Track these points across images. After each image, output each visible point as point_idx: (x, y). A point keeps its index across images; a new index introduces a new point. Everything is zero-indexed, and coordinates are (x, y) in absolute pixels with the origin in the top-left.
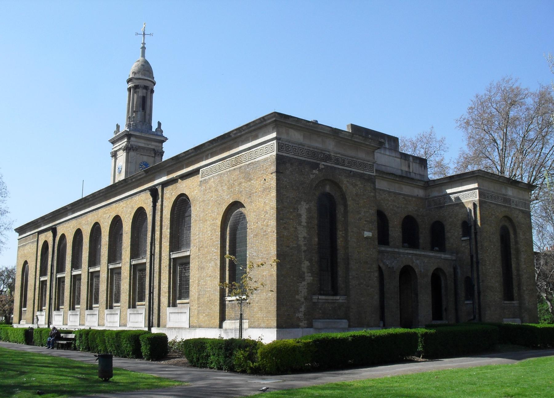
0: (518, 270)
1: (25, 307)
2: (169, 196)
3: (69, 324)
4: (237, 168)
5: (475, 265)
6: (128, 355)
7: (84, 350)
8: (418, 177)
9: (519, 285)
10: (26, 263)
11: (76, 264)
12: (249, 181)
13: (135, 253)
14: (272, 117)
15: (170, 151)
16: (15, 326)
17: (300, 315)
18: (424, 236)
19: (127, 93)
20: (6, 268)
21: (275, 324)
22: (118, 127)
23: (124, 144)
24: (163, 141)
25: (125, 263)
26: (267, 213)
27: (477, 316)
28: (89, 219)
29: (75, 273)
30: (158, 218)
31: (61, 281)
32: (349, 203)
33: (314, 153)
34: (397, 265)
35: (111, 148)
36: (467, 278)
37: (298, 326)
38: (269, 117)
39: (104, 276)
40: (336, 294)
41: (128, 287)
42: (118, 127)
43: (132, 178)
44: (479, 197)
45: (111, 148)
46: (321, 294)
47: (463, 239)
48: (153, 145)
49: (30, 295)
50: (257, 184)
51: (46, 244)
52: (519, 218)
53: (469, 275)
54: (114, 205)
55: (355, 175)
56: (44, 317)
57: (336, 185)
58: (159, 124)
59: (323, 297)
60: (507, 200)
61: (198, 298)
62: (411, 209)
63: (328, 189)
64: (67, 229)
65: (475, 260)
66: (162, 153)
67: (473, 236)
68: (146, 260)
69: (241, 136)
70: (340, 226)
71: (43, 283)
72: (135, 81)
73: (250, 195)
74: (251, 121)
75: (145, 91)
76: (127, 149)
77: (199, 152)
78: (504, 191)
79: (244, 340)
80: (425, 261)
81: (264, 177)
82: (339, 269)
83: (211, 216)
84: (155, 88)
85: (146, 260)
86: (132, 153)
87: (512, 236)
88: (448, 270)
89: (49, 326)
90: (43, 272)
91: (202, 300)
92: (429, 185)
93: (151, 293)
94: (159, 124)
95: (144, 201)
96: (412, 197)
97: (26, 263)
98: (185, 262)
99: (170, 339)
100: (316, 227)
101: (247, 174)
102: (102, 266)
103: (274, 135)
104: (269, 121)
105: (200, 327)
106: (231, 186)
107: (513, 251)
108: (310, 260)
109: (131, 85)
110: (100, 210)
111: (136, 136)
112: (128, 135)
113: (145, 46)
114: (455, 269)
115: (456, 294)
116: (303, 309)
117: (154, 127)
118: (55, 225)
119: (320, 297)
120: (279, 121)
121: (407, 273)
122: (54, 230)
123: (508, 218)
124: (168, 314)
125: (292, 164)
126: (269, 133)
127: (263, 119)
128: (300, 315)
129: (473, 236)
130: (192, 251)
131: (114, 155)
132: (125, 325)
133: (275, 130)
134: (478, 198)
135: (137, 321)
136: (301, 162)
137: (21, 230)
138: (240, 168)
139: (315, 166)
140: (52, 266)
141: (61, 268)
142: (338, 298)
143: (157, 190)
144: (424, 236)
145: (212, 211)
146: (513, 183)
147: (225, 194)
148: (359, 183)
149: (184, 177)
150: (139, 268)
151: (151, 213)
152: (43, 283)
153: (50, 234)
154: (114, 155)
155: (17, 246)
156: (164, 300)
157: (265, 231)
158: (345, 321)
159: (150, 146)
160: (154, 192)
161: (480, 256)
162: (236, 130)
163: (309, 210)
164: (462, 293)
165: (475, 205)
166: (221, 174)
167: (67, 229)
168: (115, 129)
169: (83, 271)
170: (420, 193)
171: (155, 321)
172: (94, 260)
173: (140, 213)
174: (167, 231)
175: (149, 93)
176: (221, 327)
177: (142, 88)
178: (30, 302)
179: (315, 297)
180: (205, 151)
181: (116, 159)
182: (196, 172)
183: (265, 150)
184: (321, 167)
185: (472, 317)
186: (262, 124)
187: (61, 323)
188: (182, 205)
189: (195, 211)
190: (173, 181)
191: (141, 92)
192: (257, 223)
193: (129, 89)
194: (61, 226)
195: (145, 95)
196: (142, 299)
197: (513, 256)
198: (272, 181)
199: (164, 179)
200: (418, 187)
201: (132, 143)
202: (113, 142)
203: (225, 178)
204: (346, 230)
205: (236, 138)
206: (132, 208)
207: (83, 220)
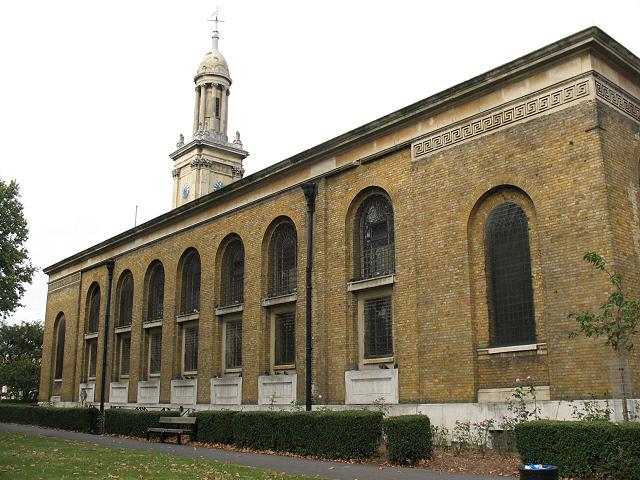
1: (59, 375)
2: (338, 202)
3: (174, 400)
4: (501, 132)
7: (394, 461)
12: (533, 148)
19: (195, 94)
20: (27, 324)
22: (182, 137)
23: (194, 159)
24: (243, 157)
26: (583, 197)
31: (126, 338)
35: (172, 165)
38: (550, 49)
42: (182, 137)
45: (172, 165)
49: (67, 360)
50: (551, 152)
51: (95, 287)
54: (225, 220)
58: (238, 134)
61: (420, 354)
73: (536, 173)
74: (474, 76)
84: (231, 89)
86: (204, 171)
89: (102, 406)
90: (92, 326)
91: (429, 356)
94: (238, 134)
99: (433, 423)
109: (201, 82)
110: (198, 230)
112: (200, 146)
113: (219, 35)
118: (112, 259)
120: (597, 45)
122: (110, 265)
124: (347, 381)
132: (255, 403)
138: (508, 130)
140: (107, 317)
141: (125, 318)
145: (444, 207)
147: (475, 176)
157: (581, 229)
160: (310, 191)
166: (463, 145)
173: (282, 228)
175: (224, 94)
176: (475, 400)
177: (214, 87)
178: (67, 371)
187: (125, 400)
191: (213, 93)
193: (199, 89)
195: (219, 97)
201: (205, 157)
206: (263, 219)
207: (165, 248)
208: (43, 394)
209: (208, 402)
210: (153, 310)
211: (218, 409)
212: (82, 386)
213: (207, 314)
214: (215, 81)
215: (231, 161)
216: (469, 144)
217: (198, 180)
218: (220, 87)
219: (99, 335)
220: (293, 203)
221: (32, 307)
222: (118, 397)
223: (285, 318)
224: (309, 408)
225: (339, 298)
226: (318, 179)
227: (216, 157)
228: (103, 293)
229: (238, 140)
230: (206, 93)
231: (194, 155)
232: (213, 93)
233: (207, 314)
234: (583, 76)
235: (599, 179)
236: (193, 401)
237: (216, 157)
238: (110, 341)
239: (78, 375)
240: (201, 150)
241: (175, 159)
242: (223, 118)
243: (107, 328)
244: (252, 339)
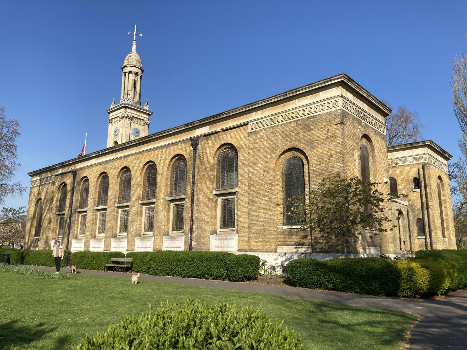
12: (310, 131)
26: (332, 157)
28: (116, 164)
36: (419, 219)
47: (414, 190)
53: (421, 217)
65: (425, 206)
67: (423, 189)
73: (310, 143)
81: (327, 127)
83: (262, 160)
91: (253, 229)
102: (131, 202)
122: (75, 173)
129: (423, 189)
137: (34, 174)
145: (264, 156)
161: (430, 204)
192: (320, 165)
206: (168, 154)
216: (278, 126)
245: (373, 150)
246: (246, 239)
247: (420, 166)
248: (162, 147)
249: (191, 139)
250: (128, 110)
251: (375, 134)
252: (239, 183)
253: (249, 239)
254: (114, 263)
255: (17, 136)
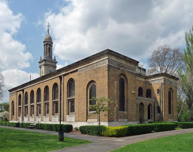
0: (173, 105)
1: (13, 115)
2: (66, 79)
5: (161, 103)
6: (89, 132)
8: (143, 75)
9: (173, 109)
10: (13, 101)
11: (32, 101)
13: (54, 97)
14: (107, 51)
15: (59, 67)
16: (11, 122)
17: (115, 117)
18: (144, 93)
19: (44, 46)
21: (108, 120)
22: (41, 57)
24: (57, 63)
25: (50, 101)
27: (161, 118)
29: (19, 106)
30: (62, 86)
31: (27, 107)
32: (128, 82)
33: (119, 64)
34: (139, 102)
37: (114, 121)
39: (42, 105)
40: (124, 111)
41: (52, 109)
42: (41, 57)
43: (47, 75)
44: (164, 81)
46: (120, 111)
48: (53, 64)
49: (15, 111)
50: (100, 74)
51: (20, 95)
52: (174, 88)
55: (131, 72)
56: (21, 118)
57: (124, 75)
58: (55, 57)
59: (121, 112)
60: (171, 83)
61: (78, 112)
62: (141, 85)
63: (122, 77)
64: (28, 90)
65: (161, 101)
66: (56, 67)
68: (58, 100)
69: (94, 58)
70: (125, 89)
71: (20, 108)
72: (46, 42)
73: (97, 78)
75: (50, 46)
76: (45, 65)
77: (77, 64)
78: (170, 80)
79: (101, 126)
80: (146, 101)
82: (125, 103)
84: (53, 45)
85: (58, 100)
86: (46, 66)
87: (172, 94)
88: (152, 104)
90: (20, 104)
91: (79, 113)
92: (146, 78)
93: (60, 110)
94: (55, 57)
95: (57, 81)
96: (142, 81)
97: (13, 101)
98: (72, 101)
100: (119, 89)
101: (96, 71)
103: (107, 57)
104: (105, 53)
105: (79, 121)
106: (90, 76)
107: (171, 99)
108: (117, 100)
109: (45, 43)
111: (47, 61)
112: (45, 60)
114: (154, 104)
115: (154, 111)
116: (115, 116)
117: (53, 58)
119: (120, 112)
120: (109, 52)
121: (142, 104)
122: (23, 91)
123: (171, 88)
124: (67, 117)
125: (112, 68)
126: (105, 57)
127: (103, 52)
128: (115, 117)
130: (76, 97)
131: (40, 67)
133: (107, 56)
134: (163, 82)
135: (55, 121)
136: (115, 67)
137: (10, 91)
139: (119, 69)
140: (23, 102)
141: (26, 103)
142: (125, 112)
143: (61, 77)
144: (144, 93)
146: (173, 77)
148: (131, 75)
149: (71, 73)
150: (55, 102)
151: (60, 85)
152: (20, 108)
153: (22, 92)
154: (40, 67)
155: (9, 96)
156: (65, 113)
158: (127, 119)
159: (52, 64)
160: (61, 78)
162: (92, 56)
163: (117, 83)
164: (156, 111)
165: (162, 84)
167: (28, 90)
168: (40, 58)
169: (35, 104)
170: (144, 80)
171: (62, 119)
172: (32, 101)
173: (55, 85)
174: (66, 90)
176: (87, 121)
179: (119, 112)
180: (80, 63)
181: (41, 68)
182: (77, 71)
183: (104, 62)
184: (121, 69)
185: (159, 119)
186: (103, 54)
188: (71, 82)
189: (76, 84)
190: (68, 74)
191: (48, 46)
193: (44, 45)
194: (26, 89)
196: (57, 112)
197: (171, 100)
198: (106, 73)
199: (65, 73)
200: (143, 78)
202: (40, 63)
203: (88, 72)
204: (127, 91)
205: (92, 59)
208: (10, 119)
209: (43, 121)
210: (46, 98)
211: (45, 123)
212: (18, 117)
213: (42, 102)
214: (49, 43)
215: (53, 64)
216: (87, 71)
217: (45, 69)
218: (50, 45)
219: (21, 106)
220: (58, 80)
221: (6, 99)
222: (26, 120)
223: (56, 103)
224: (99, 125)
225: (66, 101)
226: (62, 75)
227: (49, 63)
228: (22, 97)
229: (55, 59)
230: (46, 46)
231: (44, 63)
232: (48, 46)
233: (42, 102)
234: (106, 59)
235: (107, 81)
236: (40, 121)
237: (49, 63)
238: (24, 107)
239: (18, 115)
240: (45, 62)
241: (39, 63)
242: (51, 53)
243: (23, 104)
244: (51, 108)
245: (127, 80)
246: (77, 117)
247: (161, 84)
248: (47, 80)
249: (59, 76)
250: (46, 62)
251: (128, 73)
252: (75, 95)
253: (78, 117)
254: (31, 126)
255: (57, 49)
